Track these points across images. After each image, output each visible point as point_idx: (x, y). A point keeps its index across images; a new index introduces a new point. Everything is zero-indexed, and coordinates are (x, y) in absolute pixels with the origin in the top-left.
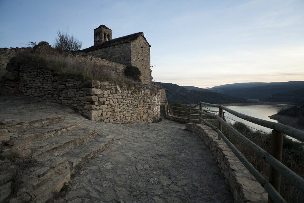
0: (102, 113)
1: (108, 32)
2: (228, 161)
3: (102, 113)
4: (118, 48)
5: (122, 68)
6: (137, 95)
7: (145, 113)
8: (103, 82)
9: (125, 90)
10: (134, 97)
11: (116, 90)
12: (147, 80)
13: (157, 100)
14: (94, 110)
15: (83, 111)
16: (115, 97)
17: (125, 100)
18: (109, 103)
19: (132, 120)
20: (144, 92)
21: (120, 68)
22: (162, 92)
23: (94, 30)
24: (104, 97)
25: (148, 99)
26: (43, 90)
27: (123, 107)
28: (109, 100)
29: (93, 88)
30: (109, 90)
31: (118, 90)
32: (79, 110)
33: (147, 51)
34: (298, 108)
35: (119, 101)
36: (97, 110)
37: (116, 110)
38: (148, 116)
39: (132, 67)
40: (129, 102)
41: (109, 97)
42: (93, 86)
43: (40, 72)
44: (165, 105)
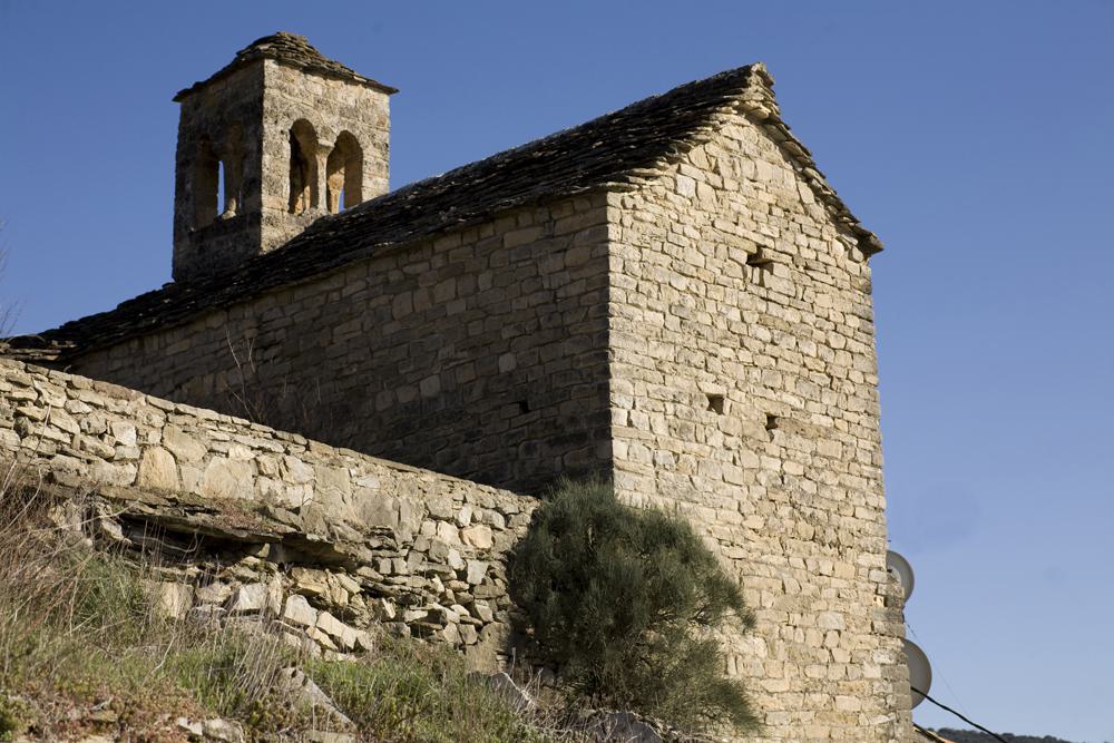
21: (447, 532)
23: (181, 96)
33: (823, 301)
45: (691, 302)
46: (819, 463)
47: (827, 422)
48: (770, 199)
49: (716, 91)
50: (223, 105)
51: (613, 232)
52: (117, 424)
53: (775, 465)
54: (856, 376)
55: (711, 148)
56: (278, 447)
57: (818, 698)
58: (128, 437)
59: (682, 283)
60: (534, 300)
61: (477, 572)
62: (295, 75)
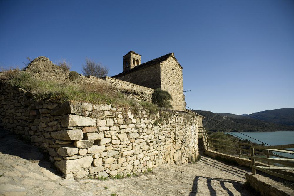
1: (137, 57)
4: (146, 72)
5: (150, 93)
6: (164, 126)
7: (177, 151)
8: (98, 106)
9: (144, 119)
11: (126, 119)
13: (193, 131)
14: (72, 158)
16: (123, 131)
17: (143, 134)
18: (111, 142)
19: (156, 165)
20: (175, 121)
21: (147, 92)
22: (198, 121)
23: (124, 56)
24: (98, 131)
25: (181, 131)
27: (139, 146)
28: (110, 136)
29: (74, 114)
30: (111, 118)
31: (131, 119)
32: (50, 156)
33: (178, 73)
34: (30, 101)
35: (131, 137)
36: (79, 157)
37: (125, 154)
38: (181, 155)
39: (161, 91)
40: (150, 137)
41: (111, 132)
42: (72, 110)
44: (203, 137)
52: (120, 83)
56: (133, 85)
59: (167, 71)
61: (150, 96)
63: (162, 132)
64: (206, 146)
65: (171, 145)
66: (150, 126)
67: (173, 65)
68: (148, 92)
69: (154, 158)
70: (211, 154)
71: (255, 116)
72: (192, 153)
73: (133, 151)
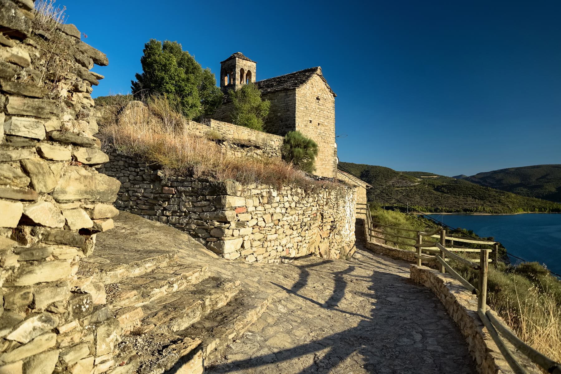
0: (243, 243)
2: (494, 363)
3: (243, 243)
5: (277, 143)
6: (309, 205)
7: (324, 239)
10: (303, 209)
12: (328, 167)
15: (208, 239)
17: (286, 215)
18: (257, 224)
20: (324, 195)
21: (273, 143)
23: (221, 63)
25: (331, 210)
26: (133, 196)
27: (282, 229)
28: (256, 217)
29: (229, 195)
33: (327, 105)
36: (234, 238)
40: (293, 219)
41: (257, 212)
42: (229, 191)
43: (130, 162)
44: (366, 221)
45: (308, 106)
46: (325, 130)
47: (327, 124)
48: (320, 89)
49: (406, 175)
50: (229, 65)
51: (297, 95)
52: (231, 129)
53: (319, 131)
54: (332, 117)
55: (311, 81)
56: (251, 131)
57: (324, 166)
58: (232, 131)
59: (307, 103)
60: (284, 105)
61: (277, 148)
62: (241, 60)
63: (307, 212)
64: (369, 235)
65: (316, 230)
66: (293, 205)
67: (319, 91)
68: (276, 141)
69: (298, 245)
70: (376, 247)
71: (481, 179)
72: (345, 244)
73: (277, 235)
